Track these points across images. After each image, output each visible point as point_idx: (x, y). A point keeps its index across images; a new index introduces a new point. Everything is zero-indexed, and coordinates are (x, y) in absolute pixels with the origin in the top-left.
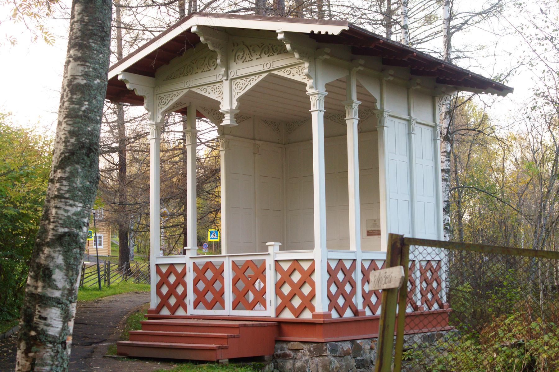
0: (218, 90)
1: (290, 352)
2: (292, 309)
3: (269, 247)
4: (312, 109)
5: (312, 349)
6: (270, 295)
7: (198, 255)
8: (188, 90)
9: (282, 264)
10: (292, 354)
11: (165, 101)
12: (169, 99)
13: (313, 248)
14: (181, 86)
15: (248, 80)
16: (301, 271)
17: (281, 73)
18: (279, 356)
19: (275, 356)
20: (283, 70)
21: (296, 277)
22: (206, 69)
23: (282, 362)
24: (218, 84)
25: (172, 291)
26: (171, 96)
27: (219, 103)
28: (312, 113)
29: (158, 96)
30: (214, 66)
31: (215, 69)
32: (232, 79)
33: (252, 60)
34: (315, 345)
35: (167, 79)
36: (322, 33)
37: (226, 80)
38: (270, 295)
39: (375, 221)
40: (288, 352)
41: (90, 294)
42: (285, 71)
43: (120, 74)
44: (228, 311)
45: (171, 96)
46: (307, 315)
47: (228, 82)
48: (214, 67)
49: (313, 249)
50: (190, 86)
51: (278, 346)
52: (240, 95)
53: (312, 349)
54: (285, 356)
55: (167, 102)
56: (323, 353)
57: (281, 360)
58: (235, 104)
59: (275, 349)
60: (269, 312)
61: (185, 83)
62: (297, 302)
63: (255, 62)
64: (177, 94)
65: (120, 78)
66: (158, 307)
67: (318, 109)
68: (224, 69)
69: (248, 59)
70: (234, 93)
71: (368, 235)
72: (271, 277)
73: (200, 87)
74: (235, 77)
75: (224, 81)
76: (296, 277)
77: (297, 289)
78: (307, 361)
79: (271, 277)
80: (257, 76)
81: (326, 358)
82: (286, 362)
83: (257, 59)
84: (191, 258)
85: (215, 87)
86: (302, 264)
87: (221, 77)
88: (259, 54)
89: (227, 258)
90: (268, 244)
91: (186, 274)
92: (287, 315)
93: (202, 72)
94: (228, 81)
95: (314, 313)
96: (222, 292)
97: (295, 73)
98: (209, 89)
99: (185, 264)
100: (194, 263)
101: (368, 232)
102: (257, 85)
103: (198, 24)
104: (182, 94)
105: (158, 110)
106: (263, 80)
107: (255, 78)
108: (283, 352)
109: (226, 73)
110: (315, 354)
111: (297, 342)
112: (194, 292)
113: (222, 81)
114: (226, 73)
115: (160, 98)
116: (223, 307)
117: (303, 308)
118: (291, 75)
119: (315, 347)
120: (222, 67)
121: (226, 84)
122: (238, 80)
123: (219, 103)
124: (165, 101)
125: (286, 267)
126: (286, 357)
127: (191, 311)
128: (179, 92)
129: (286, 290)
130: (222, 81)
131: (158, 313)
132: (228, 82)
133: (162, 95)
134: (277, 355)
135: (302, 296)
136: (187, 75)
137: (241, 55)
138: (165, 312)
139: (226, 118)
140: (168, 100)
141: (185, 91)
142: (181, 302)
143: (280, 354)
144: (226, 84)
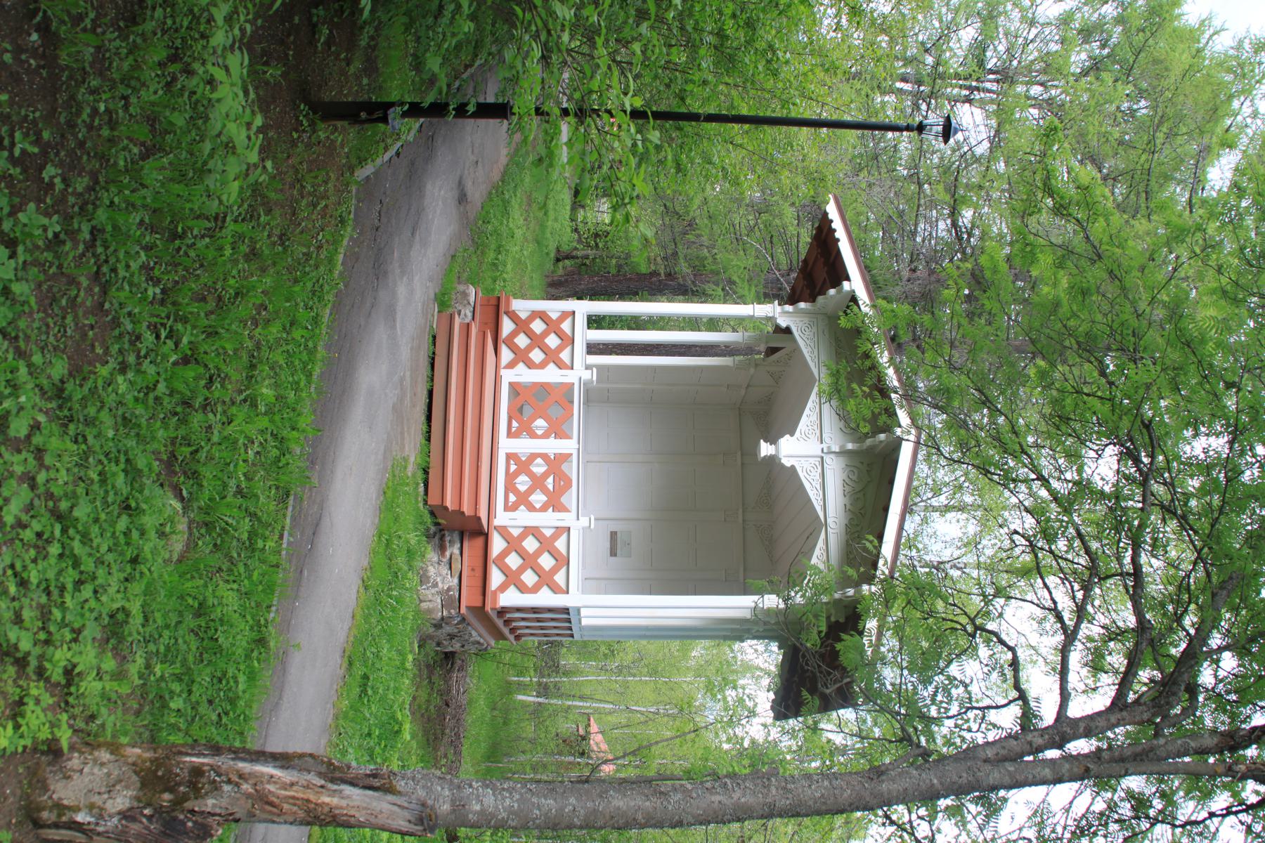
2: (505, 554)
6: (523, 518)
9: (564, 537)
13: (583, 593)
16: (560, 349)
17: (820, 544)
18: (442, 538)
21: (552, 341)
25: (537, 341)
27: (792, 435)
38: (523, 518)
40: (448, 554)
41: (537, 31)
44: (506, 445)
46: (496, 578)
51: (456, 536)
54: (442, 548)
58: (787, 462)
59: (452, 530)
60: (502, 518)
72: (547, 520)
76: (546, 561)
77: (530, 561)
78: (435, 585)
79: (547, 520)
92: (497, 545)
98: (814, 418)
102: (809, 500)
106: (818, 517)
117: (505, 570)
123: (792, 435)
125: (566, 326)
127: (508, 376)
129: (538, 326)
131: (507, 313)
132: (820, 453)
133: (815, 329)
135: (529, 348)
138: (507, 326)
142: (521, 357)
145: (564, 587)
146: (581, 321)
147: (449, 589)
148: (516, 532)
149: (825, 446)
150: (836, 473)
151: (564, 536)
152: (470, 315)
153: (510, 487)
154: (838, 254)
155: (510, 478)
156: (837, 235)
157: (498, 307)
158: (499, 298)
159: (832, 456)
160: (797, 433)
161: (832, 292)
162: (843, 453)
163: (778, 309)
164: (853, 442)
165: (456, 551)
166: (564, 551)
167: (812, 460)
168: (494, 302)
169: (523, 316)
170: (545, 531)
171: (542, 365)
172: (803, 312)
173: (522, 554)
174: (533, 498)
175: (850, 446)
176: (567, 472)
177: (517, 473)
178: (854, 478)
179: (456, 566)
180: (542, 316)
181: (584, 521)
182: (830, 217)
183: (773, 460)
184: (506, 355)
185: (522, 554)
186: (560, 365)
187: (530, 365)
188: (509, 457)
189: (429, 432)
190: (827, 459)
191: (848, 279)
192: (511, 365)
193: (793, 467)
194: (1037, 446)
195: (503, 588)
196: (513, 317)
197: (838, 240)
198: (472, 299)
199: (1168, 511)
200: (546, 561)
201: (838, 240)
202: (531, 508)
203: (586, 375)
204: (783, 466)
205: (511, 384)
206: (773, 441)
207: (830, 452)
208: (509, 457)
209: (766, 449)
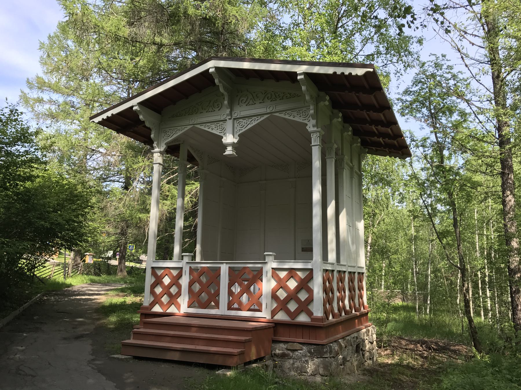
0: (221, 127)
1: (289, 352)
2: (288, 312)
3: (267, 258)
4: (313, 144)
5: (312, 350)
8: (193, 126)
10: (291, 354)
11: (169, 134)
12: (174, 132)
13: (312, 259)
14: (187, 122)
15: (250, 120)
17: (282, 115)
19: (273, 355)
20: (284, 113)
22: (211, 110)
24: (221, 123)
26: (176, 130)
30: (218, 107)
31: (219, 110)
32: (234, 119)
33: (255, 104)
34: (315, 347)
37: (230, 119)
39: (309, 241)
42: (286, 114)
43: (135, 106)
44: (222, 310)
45: (176, 130)
46: (303, 318)
47: (231, 121)
48: (219, 108)
50: (195, 123)
52: (241, 132)
53: (312, 350)
61: (191, 120)
64: (181, 129)
65: (134, 108)
66: (150, 304)
67: (318, 144)
68: (229, 110)
70: (235, 130)
71: (302, 251)
73: (204, 125)
74: (238, 117)
75: (228, 120)
80: (259, 117)
81: (327, 359)
82: (285, 361)
84: (187, 263)
85: (218, 125)
87: (225, 116)
89: (225, 264)
90: (266, 253)
91: (182, 276)
92: (281, 316)
93: (207, 112)
94: (231, 120)
95: (312, 317)
96: (217, 294)
98: (213, 126)
99: (182, 268)
100: (190, 267)
101: (302, 248)
102: (258, 124)
105: (162, 141)
107: (257, 119)
109: (231, 114)
113: (226, 120)
114: (231, 114)
115: (165, 131)
116: (217, 306)
117: (298, 312)
119: (316, 349)
120: (228, 108)
121: (229, 123)
122: (241, 120)
124: (169, 134)
128: (183, 127)
132: (231, 121)
133: (167, 130)
134: (275, 354)
137: (245, 99)
138: (157, 309)
139: (228, 149)
141: (189, 127)
143: (278, 353)
144: (229, 123)
149: (227, 119)
150: (241, 111)
159: (233, 113)
160: (221, 134)
161: (141, 117)
162: (231, 106)
167: (236, 125)
176: (311, 287)
182: (100, 120)
184: (172, 309)
186: (180, 276)
188: (230, 308)
190: (234, 116)
191: (132, 107)
195: (310, 314)
199: (326, 46)
201: (112, 114)
208: (230, 308)
209: (229, 151)
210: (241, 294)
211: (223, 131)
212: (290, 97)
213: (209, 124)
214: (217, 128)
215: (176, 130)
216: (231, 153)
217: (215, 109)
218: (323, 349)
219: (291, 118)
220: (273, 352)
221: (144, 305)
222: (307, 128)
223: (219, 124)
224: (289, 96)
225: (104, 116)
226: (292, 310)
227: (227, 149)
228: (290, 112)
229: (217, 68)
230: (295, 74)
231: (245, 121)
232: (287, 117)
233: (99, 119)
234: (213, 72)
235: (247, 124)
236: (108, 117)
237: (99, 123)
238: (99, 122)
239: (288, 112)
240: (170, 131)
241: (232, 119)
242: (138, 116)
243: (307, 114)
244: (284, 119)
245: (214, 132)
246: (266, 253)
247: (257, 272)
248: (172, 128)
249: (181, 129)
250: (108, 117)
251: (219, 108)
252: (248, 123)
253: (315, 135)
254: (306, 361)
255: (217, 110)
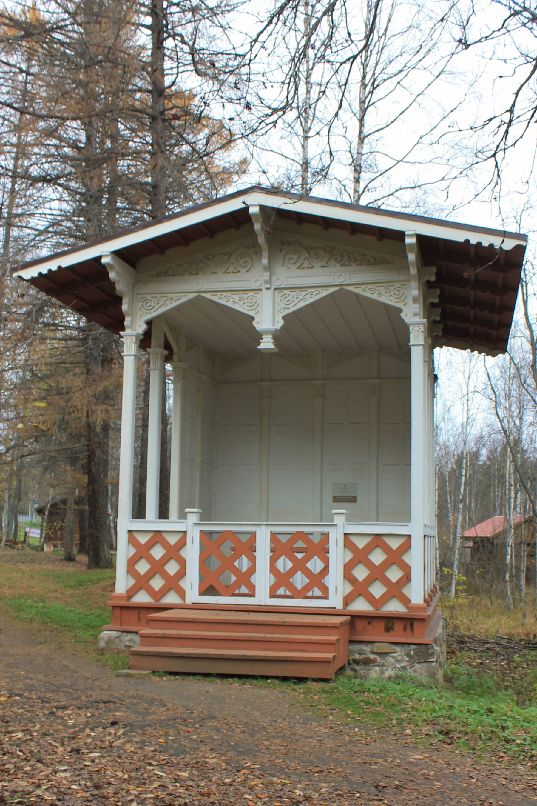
0: (250, 301)
3: (336, 517)
5: (412, 652)
7: (201, 520)
8: (197, 294)
9: (354, 539)
10: (379, 659)
12: (161, 303)
15: (303, 293)
16: (386, 549)
17: (359, 291)
22: (231, 269)
23: (363, 670)
27: (401, 311)
28: (412, 348)
29: (140, 296)
31: (247, 271)
32: (275, 289)
33: (313, 267)
35: (158, 275)
36: (471, 242)
37: (267, 289)
40: (372, 656)
48: (247, 269)
49: (410, 522)
53: (412, 652)
55: (157, 307)
56: (429, 658)
57: (362, 667)
58: (279, 324)
62: (157, 583)
63: (318, 270)
64: (175, 298)
69: (306, 264)
70: (277, 308)
73: (219, 294)
74: (283, 286)
75: (263, 289)
76: (158, 552)
80: (320, 290)
82: (369, 670)
83: (322, 267)
86: (166, 536)
88: (325, 261)
89: (263, 527)
90: (187, 510)
93: (224, 272)
97: (237, 300)
98: (236, 297)
99: (186, 532)
102: (312, 305)
103: (261, 203)
104: (184, 300)
106: (331, 295)
107: (316, 292)
108: (363, 656)
110: (417, 660)
111: (385, 644)
112: (344, 577)
113: (261, 290)
117: (385, 599)
118: (376, 294)
123: (253, 318)
125: (143, 540)
126: (369, 664)
128: (179, 295)
130: (261, 290)
133: (149, 297)
135: (165, 575)
136: (197, 274)
139: (264, 340)
140: (159, 305)
145: (180, 536)
146: (138, 525)
147: (408, 655)
148: (349, 588)
149: (263, 287)
151: (136, 535)
152: (130, 636)
153: (303, 594)
154: (71, 268)
155: (296, 594)
156: (54, 268)
157: (122, 608)
158: (114, 607)
159: (274, 279)
161: (112, 275)
162: (269, 268)
163: (128, 331)
164: (261, 258)
165: (367, 648)
166: (150, 536)
167: (277, 300)
168: (117, 612)
169: (132, 582)
170: (131, 555)
171: (182, 562)
172: (131, 304)
173: (150, 575)
174: (245, 568)
175: (265, 261)
177: (291, 587)
178: (295, 258)
179: (385, 648)
180: (132, 563)
181: (339, 520)
182: (35, 275)
183: (277, 336)
184: (171, 599)
185: (150, 575)
186: (182, 543)
187: (182, 573)
189: (240, 677)
190: (276, 284)
192: (182, 594)
193: (284, 318)
194: (98, 131)
195: (405, 601)
196: (132, 592)
197: (60, 267)
198: (114, 634)
200: (158, 552)
201: (60, 267)
202: (325, 571)
203: (193, 518)
204: (283, 327)
205: (202, 593)
206: (258, 336)
207: (270, 281)
210: (292, 572)
211: (254, 307)
212: (374, 264)
213: (228, 294)
214: (242, 302)
215: (165, 299)
216: (271, 346)
217: (239, 269)
218: (428, 649)
219: (375, 297)
220: (351, 658)
221: (412, 602)
222: (402, 315)
223: (247, 296)
224: (372, 260)
225: (44, 269)
226: (377, 596)
227: (262, 339)
228: (373, 286)
229: (263, 208)
230: (400, 236)
231: (294, 293)
232: (368, 294)
233: (29, 273)
234: (255, 215)
235: (298, 300)
236: (50, 271)
237: (33, 281)
238: (32, 278)
239: (370, 286)
240: (153, 300)
241: (273, 288)
242: (107, 274)
243: (401, 293)
244: (356, 295)
245: (237, 307)
246: (335, 511)
247: (290, 536)
248: (159, 296)
249: (175, 298)
250: (50, 271)
251: (247, 269)
252: (300, 298)
253: (416, 329)
254: (402, 667)
255: (243, 271)
